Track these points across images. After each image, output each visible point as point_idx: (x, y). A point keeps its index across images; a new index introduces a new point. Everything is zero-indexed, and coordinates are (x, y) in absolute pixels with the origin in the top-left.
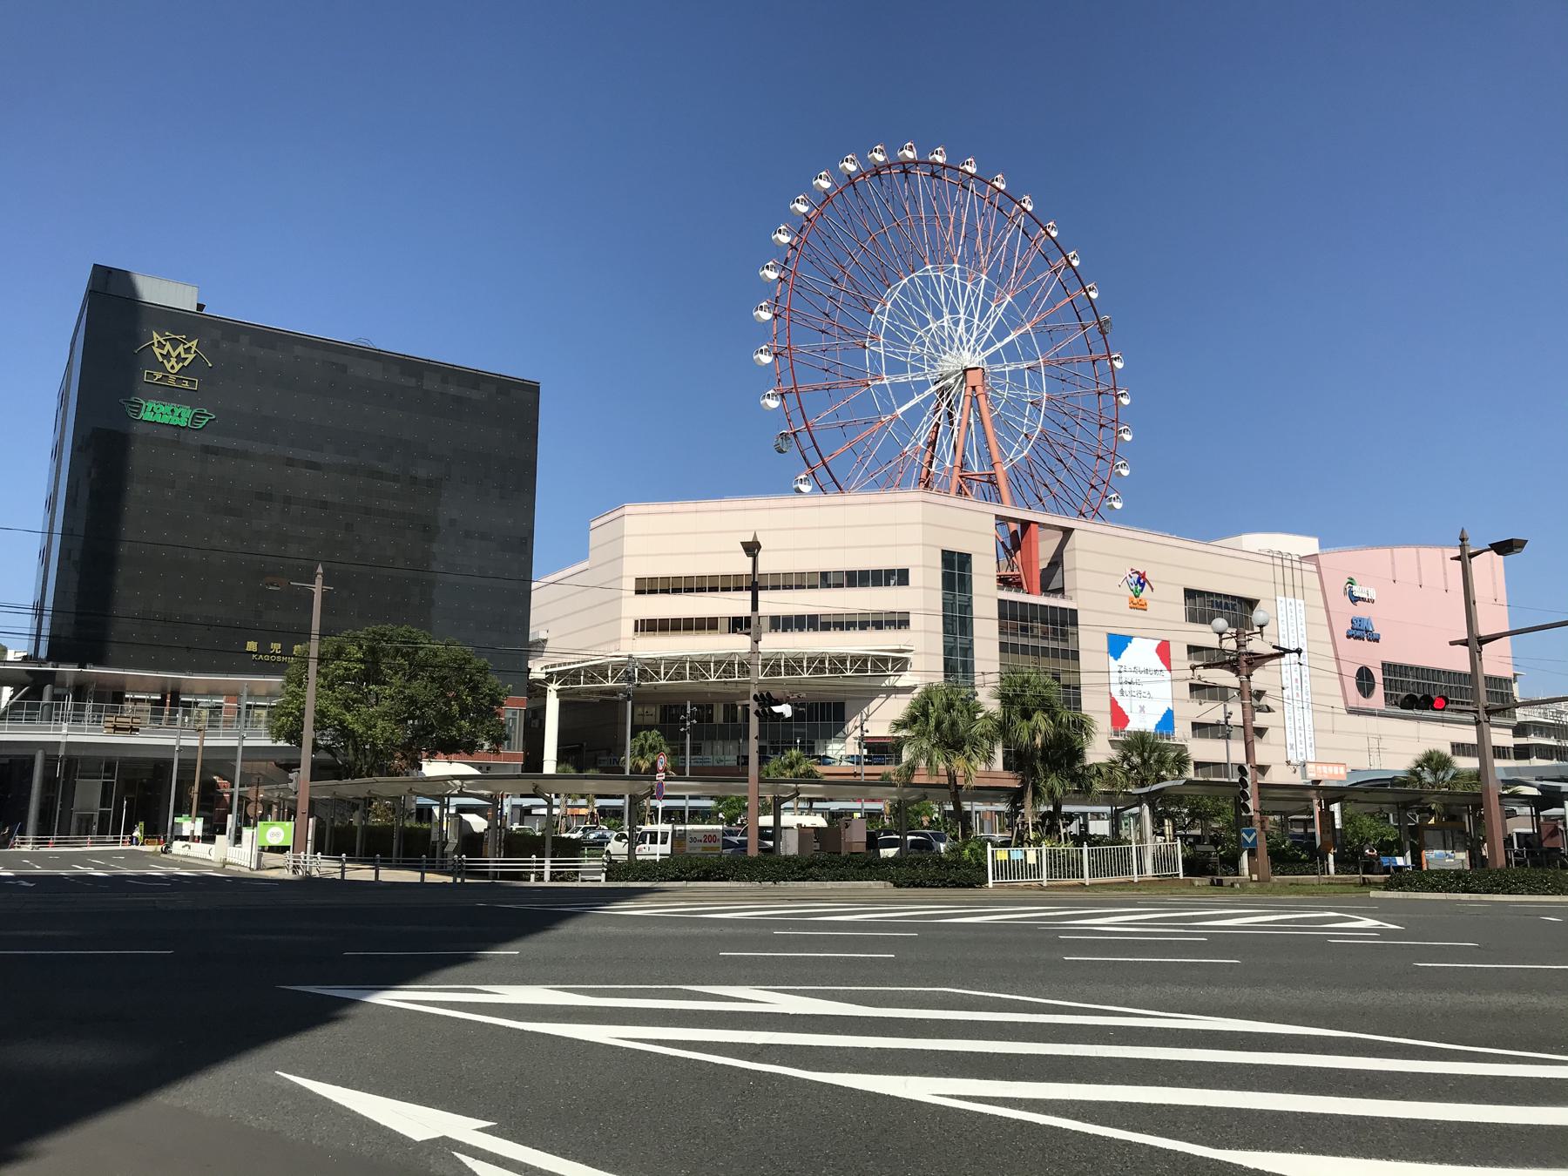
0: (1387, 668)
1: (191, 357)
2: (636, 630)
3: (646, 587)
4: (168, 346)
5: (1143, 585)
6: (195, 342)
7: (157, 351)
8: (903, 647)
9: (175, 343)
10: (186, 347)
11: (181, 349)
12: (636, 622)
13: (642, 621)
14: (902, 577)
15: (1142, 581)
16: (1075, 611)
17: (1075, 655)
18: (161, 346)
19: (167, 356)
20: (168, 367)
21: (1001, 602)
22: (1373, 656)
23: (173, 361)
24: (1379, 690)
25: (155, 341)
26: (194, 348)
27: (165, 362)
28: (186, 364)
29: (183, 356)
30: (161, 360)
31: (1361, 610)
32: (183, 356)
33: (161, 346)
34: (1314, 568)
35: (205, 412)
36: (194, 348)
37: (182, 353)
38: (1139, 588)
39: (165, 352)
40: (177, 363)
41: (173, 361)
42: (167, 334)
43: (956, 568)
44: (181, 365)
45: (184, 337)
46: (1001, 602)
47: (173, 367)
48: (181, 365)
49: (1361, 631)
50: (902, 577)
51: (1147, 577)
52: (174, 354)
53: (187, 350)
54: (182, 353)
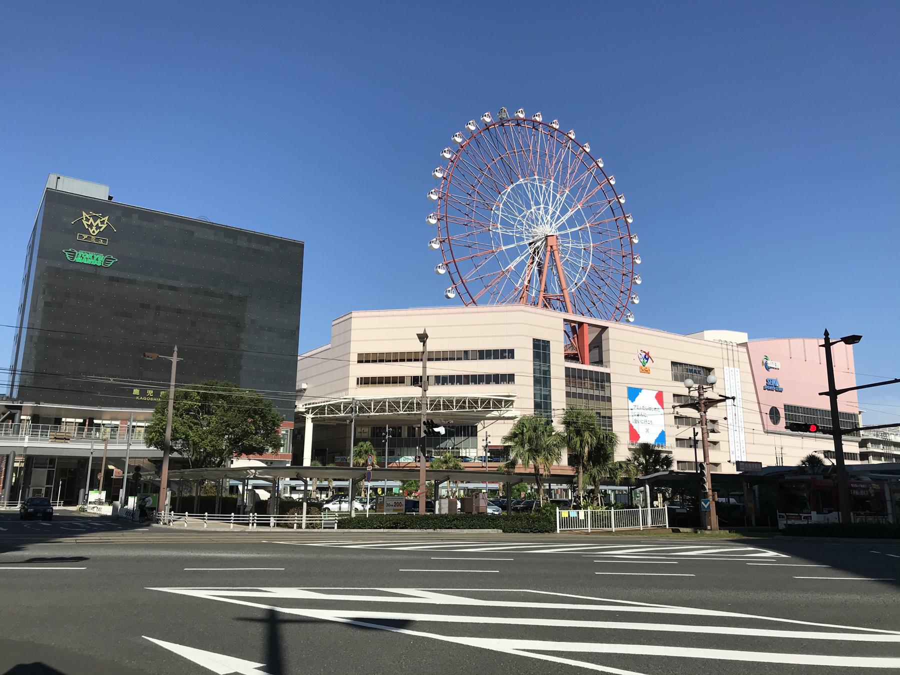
0: (787, 408)
1: (104, 226)
2: (358, 384)
3: (364, 359)
4: (91, 220)
5: (648, 359)
6: (107, 218)
7: (85, 223)
8: (510, 394)
9: (95, 219)
10: (101, 220)
11: (98, 221)
12: (358, 379)
13: (361, 378)
14: (508, 354)
15: (647, 357)
16: (608, 375)
17: (609, 399)
18: (87, 220)
19: (91, 226)
20: (91, 231)
21: (567, 369)
22: (779, 401)
23: (94, 228)
24: (783, 422)
25: (84, 217)
26: (106, 221)
27: (89, 229)
28: (101, 230)
29: (100, 225)
30: (87, 228)
31: (771, 375)
32: (100, 225)
33: (87, 220)
34: (745, 350)
35: (112, 257)
36: (106, 221)
37: (99, 224)
38: (646, 361)
39: (89, 223)
40: (96, 229)
41: (94, 228)
42: (91, 213)
43: (541, 349)
44: (98, 230)
45: (101, 215)
46: (567, 369)
47: (94, 232)
48: (98, 230)
49: (772, 386)
50: (508, 354)
51: (650, 355)
52: (95, 224)
53: (102, 222)
54: (99, 224)
